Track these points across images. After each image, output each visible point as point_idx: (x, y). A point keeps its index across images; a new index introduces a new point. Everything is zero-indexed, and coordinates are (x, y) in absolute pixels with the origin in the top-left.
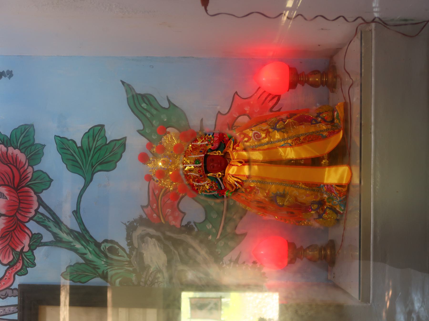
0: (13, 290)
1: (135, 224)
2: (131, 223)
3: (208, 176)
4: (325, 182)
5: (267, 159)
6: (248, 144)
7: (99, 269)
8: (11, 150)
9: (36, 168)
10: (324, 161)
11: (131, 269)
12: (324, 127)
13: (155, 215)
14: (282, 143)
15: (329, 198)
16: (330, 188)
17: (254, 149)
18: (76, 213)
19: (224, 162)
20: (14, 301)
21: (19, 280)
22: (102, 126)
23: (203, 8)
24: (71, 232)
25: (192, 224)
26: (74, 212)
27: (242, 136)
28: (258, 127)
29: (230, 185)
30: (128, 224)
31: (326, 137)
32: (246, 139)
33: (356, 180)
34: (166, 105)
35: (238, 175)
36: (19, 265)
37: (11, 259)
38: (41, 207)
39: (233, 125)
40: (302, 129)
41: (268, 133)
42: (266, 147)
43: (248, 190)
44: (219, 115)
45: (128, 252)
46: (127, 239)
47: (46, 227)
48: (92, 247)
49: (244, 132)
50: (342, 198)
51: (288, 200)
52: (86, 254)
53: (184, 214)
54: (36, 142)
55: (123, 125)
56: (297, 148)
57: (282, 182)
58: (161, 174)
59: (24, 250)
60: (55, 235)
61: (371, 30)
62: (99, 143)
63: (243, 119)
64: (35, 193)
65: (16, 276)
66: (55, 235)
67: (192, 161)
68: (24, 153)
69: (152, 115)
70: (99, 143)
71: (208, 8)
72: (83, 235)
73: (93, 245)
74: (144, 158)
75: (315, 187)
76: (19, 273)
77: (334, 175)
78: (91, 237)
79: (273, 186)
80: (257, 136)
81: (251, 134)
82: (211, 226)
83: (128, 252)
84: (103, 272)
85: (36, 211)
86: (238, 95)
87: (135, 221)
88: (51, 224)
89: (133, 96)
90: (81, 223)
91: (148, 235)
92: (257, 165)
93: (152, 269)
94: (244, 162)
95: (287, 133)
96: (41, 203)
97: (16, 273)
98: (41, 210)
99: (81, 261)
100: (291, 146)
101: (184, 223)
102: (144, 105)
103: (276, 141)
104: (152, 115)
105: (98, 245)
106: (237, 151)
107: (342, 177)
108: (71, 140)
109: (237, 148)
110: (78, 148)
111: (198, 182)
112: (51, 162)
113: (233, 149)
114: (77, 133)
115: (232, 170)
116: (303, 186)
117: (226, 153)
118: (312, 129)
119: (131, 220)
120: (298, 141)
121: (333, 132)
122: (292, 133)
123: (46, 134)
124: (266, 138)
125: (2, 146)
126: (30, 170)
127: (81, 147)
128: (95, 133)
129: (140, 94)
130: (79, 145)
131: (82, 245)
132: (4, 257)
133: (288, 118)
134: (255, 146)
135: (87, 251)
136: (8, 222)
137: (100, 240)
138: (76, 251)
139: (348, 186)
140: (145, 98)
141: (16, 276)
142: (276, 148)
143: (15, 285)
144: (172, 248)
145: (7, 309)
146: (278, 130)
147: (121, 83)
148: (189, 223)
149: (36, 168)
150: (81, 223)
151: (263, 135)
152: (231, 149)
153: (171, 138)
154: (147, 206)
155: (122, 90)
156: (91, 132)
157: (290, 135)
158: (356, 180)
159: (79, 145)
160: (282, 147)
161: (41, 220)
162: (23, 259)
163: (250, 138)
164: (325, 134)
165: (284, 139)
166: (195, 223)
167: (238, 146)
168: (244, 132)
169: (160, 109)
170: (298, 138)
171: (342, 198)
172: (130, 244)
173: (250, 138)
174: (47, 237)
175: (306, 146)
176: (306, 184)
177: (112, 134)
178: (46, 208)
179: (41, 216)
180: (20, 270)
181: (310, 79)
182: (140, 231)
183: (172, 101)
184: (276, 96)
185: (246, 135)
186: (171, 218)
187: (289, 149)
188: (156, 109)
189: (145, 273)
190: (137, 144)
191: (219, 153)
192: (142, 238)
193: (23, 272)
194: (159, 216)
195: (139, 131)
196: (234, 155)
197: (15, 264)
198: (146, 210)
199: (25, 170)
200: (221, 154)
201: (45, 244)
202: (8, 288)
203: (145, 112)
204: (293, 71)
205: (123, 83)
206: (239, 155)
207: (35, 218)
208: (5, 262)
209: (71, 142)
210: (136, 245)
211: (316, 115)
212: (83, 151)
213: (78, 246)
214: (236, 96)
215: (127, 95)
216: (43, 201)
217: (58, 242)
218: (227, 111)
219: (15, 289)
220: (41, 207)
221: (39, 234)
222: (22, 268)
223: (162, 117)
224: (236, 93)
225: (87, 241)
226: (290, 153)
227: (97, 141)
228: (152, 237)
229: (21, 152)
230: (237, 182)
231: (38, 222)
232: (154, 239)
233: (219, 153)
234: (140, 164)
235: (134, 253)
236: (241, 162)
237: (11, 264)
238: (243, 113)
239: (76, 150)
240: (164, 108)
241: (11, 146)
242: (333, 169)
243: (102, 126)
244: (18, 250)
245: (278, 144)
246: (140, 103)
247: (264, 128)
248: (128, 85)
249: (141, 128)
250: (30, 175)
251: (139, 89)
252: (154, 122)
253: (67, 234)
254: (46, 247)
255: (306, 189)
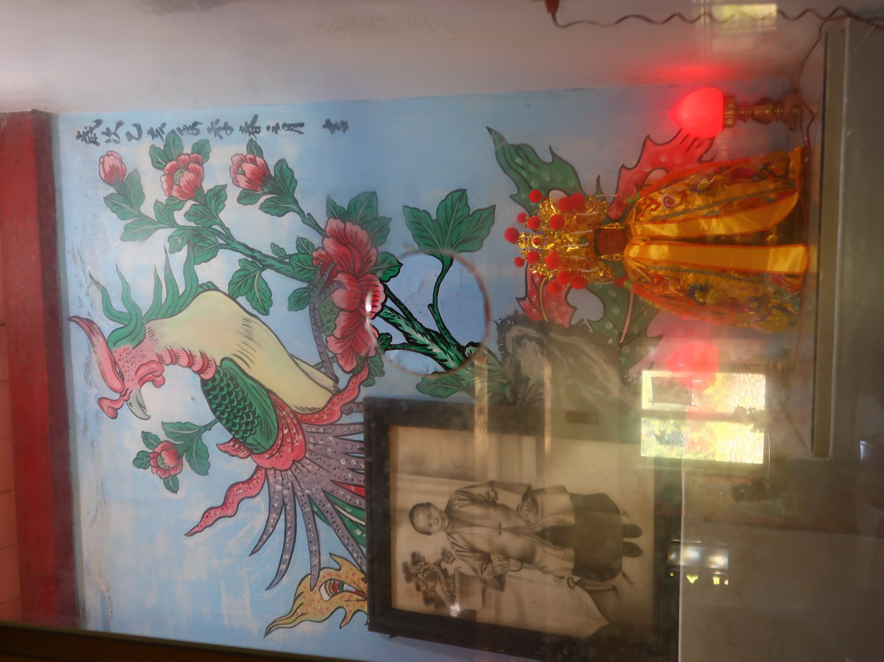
0: (358, 404)
1: (509, 322)
2: (504, 322)
3: (601, 260)
4: (769, 269)
5: (683, 234)
6: (655, 213)
7: (463, 380)
8: (349, 226)
9: (382, 249)
10: (771, 237)
11: (504, 381)
12: (772, 186)
13: (535, 310)
14: (705, 212)
15: (775, 293)
16: (778, 278)
17: (663, 221)
18: (433, 307)
19: (624, 238)
20: (359, 417)
21: (365, 392)
22: (464, 191)
23: (549, 16)
24: (427, 332)
25: (586, 322)
26: (430, 305)
27: (648, 202)
28: (670, 188)
29: (634, 271)
30: (499, 322)
31: (774, 201)
32: (653, 206)
33: (814, 268)
34: (548, 158)
35: (642, 259)
36: (365, 374)
37: (354, 366)
38: (389, 299)
39: (643, 183)
40: (737, 190)
41: (684, 195)
42: (682, 217)
43: (656, 280)
44: (623, 170)
45: (500, 359)
46: (498, 342)
47: (397, 326)
48: (453, 352)
49: (651, 195)
50: (795, 294)
51: (712, 296)
52: (446, 361)
53: (575, 308)
54: (381, 214)
55: (492, 189)
56: (726, 219)
57: (700, 269)
58: (534, 257)
59: (370, 355)
60: (406, 335)
61: (843, 31)
62: (459, 214)
63: (657, 175)
64: (382, 281)
65: (362, 387)
66: (406, 335)
67: (577, 239)
68: (365, 229)
69: (529, 173)
70: (459, 214)
71: (558, 15)
72: (442, 337)
73: (455, 349)
74: (513, 236)
75: (756, 277)
76: (365, 383)
77: (787, 260)
78: (452, 338)
79: (691, 274)
80: (669, 202)
81: (660, 199)
82: (611, 325)
83: (500, 359)
84: (469, 384)
85: (383, 304)
86: (652, 141)
87: (509, 318)
88: (402, 322)
89: (503, 148)
90: (439, 321)
91: (526, 336)
92: (669, 244)
93: (531, 383)
94: (649, 240)
95: (713, 195)
96: (389, 294)
97: (361, 383)
98: (389, 303)
99: (441, 369)
100: (717, 216)
101: (575, 321)
102: (518, 160)
103: (695, 209)
104: (529, 173)
105: (461, 349)
106: (641, 223)
107: (794, 264)
108: (424, 211)
109: (641, 219)
110: (433, 221)
111: (588, 267)
112: (399, 239)
113: (636, 220)
114: (430, 201)
115: (634, 251)
116: (736, 275)
117: (628, 227)
118: (752, 189)
119: (504, 316)
120: (728, 209)
121: (783, 195)
122: (721, 196)
123: (391, 206)
124: (680, 204)
125: (338, 221)
126: (373, 251)
127: (437, 221)
128: (454, 202)
129: (513, 145)
130: (434, 217)
131: (442, 349)
132: (346, 363)
133: (716, 173)
134: (666, 216)
135: (448, 357)
136: (349, 319)
137: (463, 343)
138: (433, 356)
139: (805, 274)
140: (520, 149)
141: (362, 387)
142: (696, 219)
143: (360, 399)
144: (558, 355)
145: (352, 427)
146: (700, 192)
147: (486, 131)
148: (581, 321)
149: (382, 249)
150: (439, 321)
151: (677, 200)
152: (633, 220)
153: (549, 206)
154: (524, 299)
155: (489, 140)
156: (449, 198)
157: (718, 199)
158: (814, 268)
159: (434, 217)
160: (704, 217)
161: (389, 316)
162: (369, 364)
163: (658, 205)
164: (772, 196)
165: (708, 206)
166: (589, 321)
167: (642, 216)
168: (651, 195)
169: (538, 163)
170: (729, 203)
171: (795, 294)
172: (503, 348)
173: (658, 205)
174: (398, 338)
175: (742, 216)
176: (738, 271)
177: (476, 202)
178: (396, 300)
179: (389, 311)
180: (366, 380)
181: (757, 112)
182: (515, 331)
183: (558, 153)
184: (707, 139)
185: (653, 201)
186: (556, 315)
187: (714, 222)
188: (535, 166)
189: (523, 387)
190: (508, 214)
191: (617, 226)
192: (518, 341)
193: (369, 382)
194: (540, 311)
195: (511, 197)
196: (638, 229)
197: (360, 372)
198: (522, 303)
199: (369, 252)
200: (620, 228)
201: (395, 347)
202: (353, 401)
203: (519, 169)
204: (727, 99)
205: (489, 130)
206: (643, 229)
207: (381, 314)
208: (348, 369)
209: (423, 213)
210: (510, 349)
211: (761, 167)
212: (439, 224)
213: (436, 350)
214: (648, 141)
215: (496, 147)
216: (391, 292)
217: (411, 344)
218: (634, 163)
219: (361, 403)
220: (389, 299)
221: (387, 334)
222: (368, 377)
223: (543, 175)
224: (648, 137)
225: (448, 345)
226: (717, 227)
227: (458, 211)
228: (530, 339)
229: (362, 229)
230: (641, 268)
231: (386, 320)
232: (534, 343)
233: (617, 226)
234: (509, 244)
235: (508, 361)
236: (645, 240)
237: (356, 371)
238: (657, 165)
239: (431, 224)
240: (546, 163)
241: (349, 221)
242: (782, 250)
243: (464, 191)
244: (363, 354)
245: (700, 212)
246: (515, 158)
247: (680, 190)
248: (496, 133)
249: (516, 192)
250: (374, 258)
251: (513, 138)
252: (532, 183)
253: (422, 334)
254: (396, 351)
255: (739, 280)
